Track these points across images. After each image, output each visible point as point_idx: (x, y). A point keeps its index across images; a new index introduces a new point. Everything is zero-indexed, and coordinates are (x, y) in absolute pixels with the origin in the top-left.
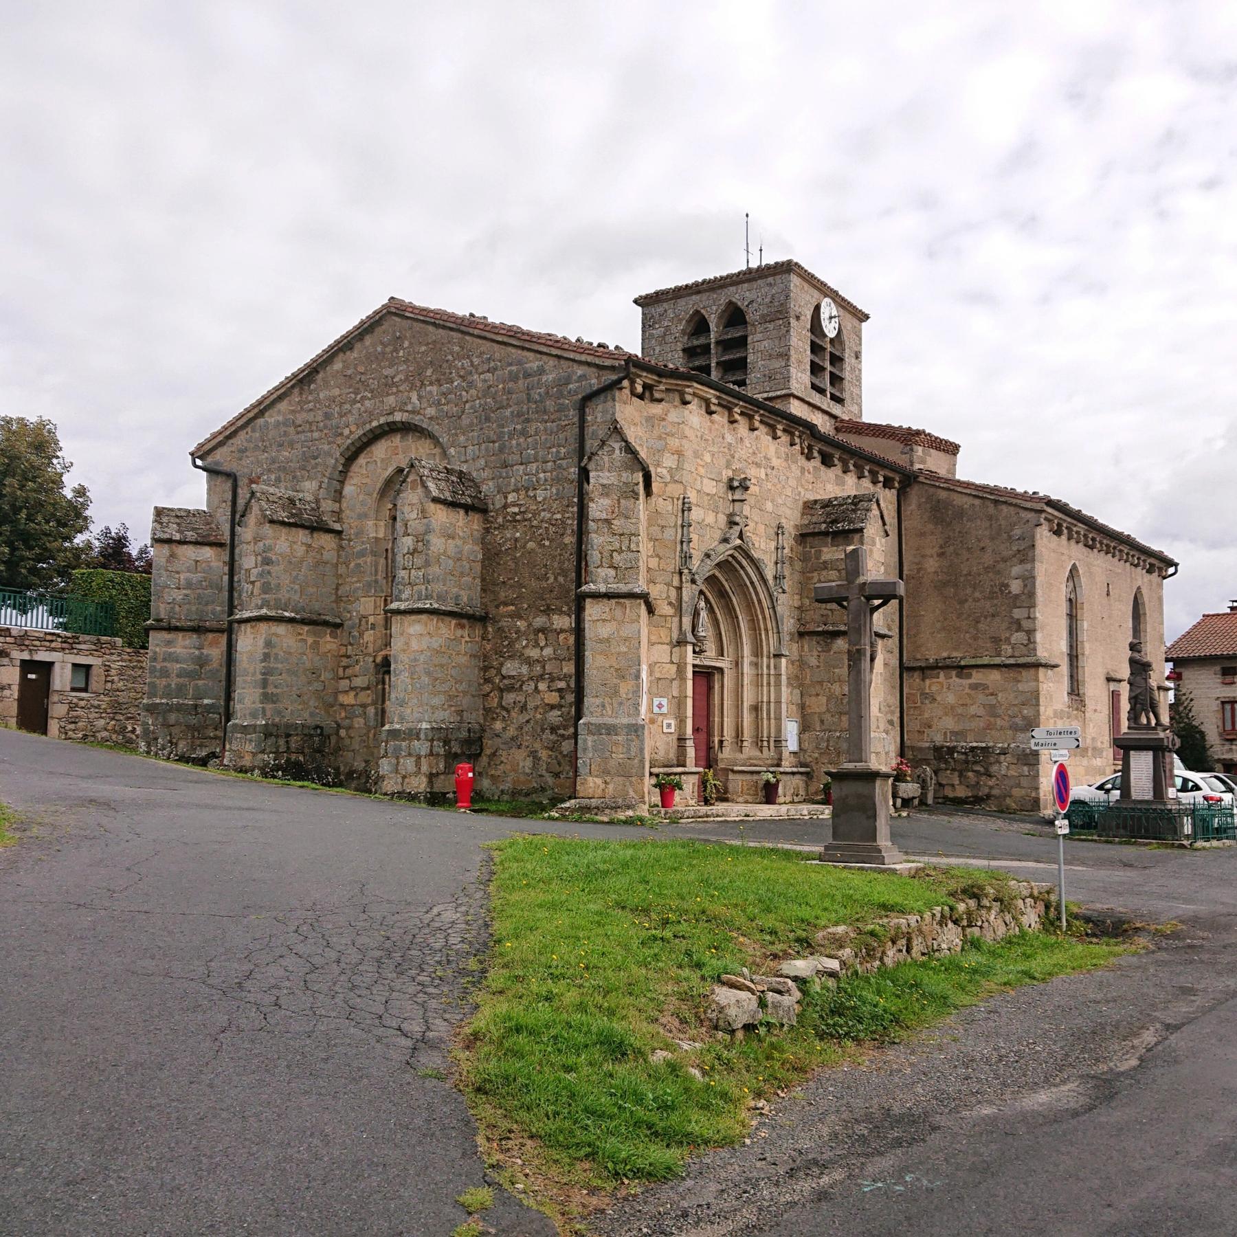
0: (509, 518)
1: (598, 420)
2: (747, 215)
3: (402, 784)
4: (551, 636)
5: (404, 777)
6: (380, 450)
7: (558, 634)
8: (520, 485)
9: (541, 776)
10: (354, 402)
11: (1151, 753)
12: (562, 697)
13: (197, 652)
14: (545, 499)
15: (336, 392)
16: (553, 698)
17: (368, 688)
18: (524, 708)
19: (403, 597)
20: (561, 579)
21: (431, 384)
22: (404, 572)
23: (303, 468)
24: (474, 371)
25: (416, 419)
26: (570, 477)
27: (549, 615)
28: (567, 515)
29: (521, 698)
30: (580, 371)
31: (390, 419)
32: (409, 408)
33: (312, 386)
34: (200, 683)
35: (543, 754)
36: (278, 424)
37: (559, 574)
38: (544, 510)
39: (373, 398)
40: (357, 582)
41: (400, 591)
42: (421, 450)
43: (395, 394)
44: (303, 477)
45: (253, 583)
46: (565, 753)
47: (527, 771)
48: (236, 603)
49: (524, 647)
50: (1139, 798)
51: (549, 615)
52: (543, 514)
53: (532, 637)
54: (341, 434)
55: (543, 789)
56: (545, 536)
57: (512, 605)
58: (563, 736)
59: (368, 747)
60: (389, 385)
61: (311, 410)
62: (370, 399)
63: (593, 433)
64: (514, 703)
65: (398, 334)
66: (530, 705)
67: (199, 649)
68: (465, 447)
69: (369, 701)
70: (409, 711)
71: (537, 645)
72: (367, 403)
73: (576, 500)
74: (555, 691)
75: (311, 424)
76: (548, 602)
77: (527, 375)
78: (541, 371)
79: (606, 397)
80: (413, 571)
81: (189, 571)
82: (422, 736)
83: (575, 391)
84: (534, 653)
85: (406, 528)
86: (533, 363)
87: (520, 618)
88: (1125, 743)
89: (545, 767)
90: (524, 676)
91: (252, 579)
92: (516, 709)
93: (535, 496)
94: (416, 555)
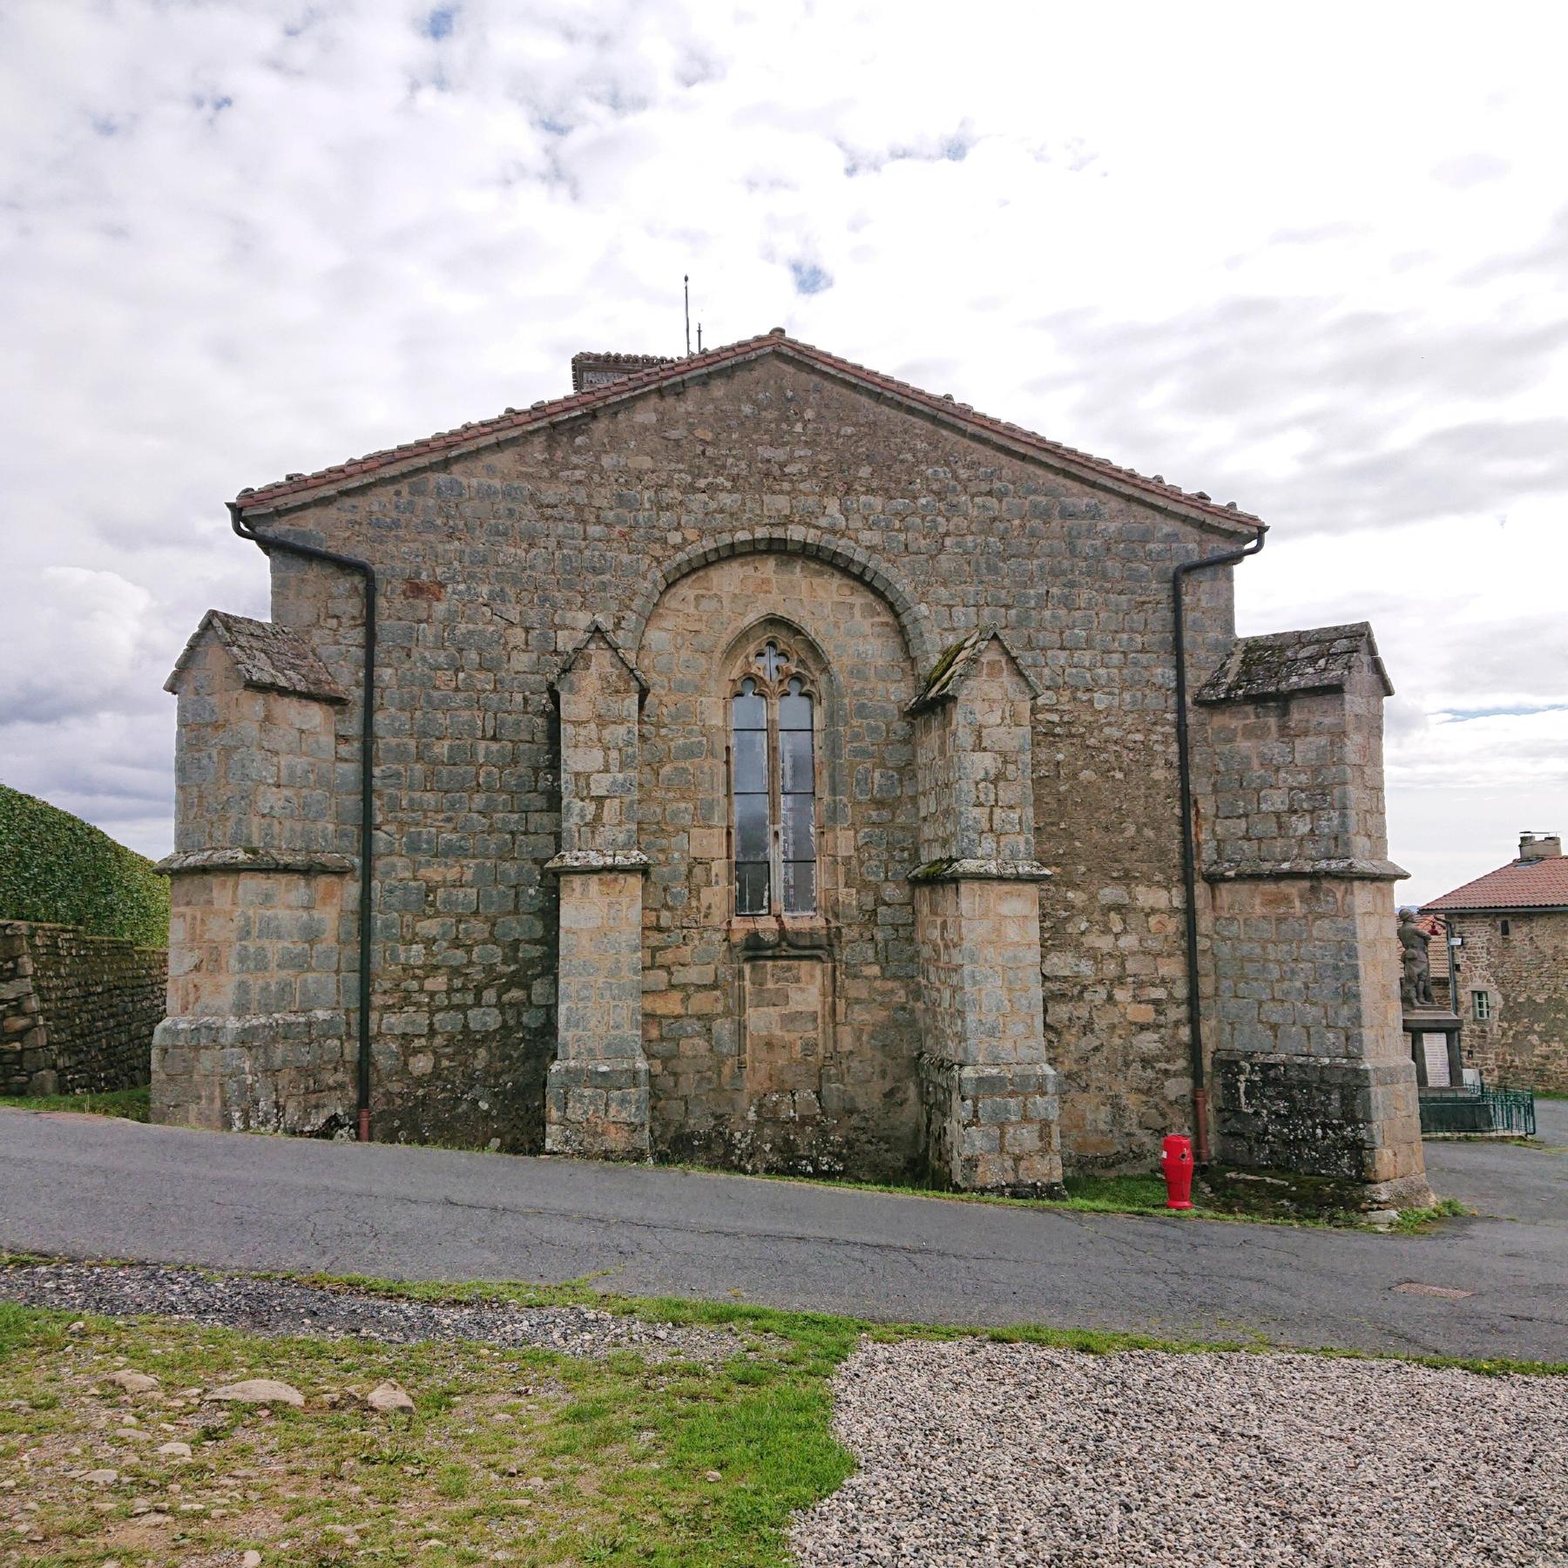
0: (1041, 729)
1: (1203, 604)
2: (686, 279)
3: (1016, 1170)
4: (1134, 921)
5: (1017, 1159)
6: (729, 579)
7: (1147, 915)
8: (1060, 681)
9: (1129, 1135)
10: (692, 489)
11: (1444, 1035)
12: (1159, 1012)
13: (305, 916)
14: (1109, 709)
16: (1146, 1014)
17: (714, 986)
18: (1088, 1028)
19: (980, 852)
20: (1149, 833)
21: (870, 491)
22: (979, 810)
24: (959, 488)
25: (841, 545)
26: (1154, 680)
27: (1128, 885)
28: (1154, 737)
29: (1083, 1012)
30: (1168, 527)
31: (778, 533)
32: (823, 522)
33: (579, 440)
34: (310, 976)
35: (1131, 1101)
37: (1145, 825)
38: (1110, 724)
40: (677, 800)
41: (971, 841)
42: (821, 593)
43: (789, 493)
44: (568, 602)
46: (1172, 1098)
47: (1102, 1126)
48: (379, 819)
49: (1083, 933)
50: (1436, 1085)
51: (1128, 885)
52: (1107, 730)
53: (1097, 916)
55: (1139, 1157)
56: (1115, 764)
57: (1057, 865)
58: (1166, 1072)
59: (719, 1089)
60: (771, 477)
61: (579, 482)
62: (729, 492)
63: (1194, 622)
64: (1070, 1019)
65: (790, 394)
66: (1101, 1023)
67: (307, 908)
68: (950, 607)
69: (720, 1008)
70: (1009, 1045)
71: (1106, 930)
72: (726, 499)
73: (1170, 717)
74: (1148, 1002)
75: (580, 509)
76: (1127, 865)
77: (1066, 514)
78: (1094, 514)
79: (1216, 574)
80: (997, 811)
81: (291, 752)
82: (1050, 1088)
83: (1159, 554)
84: (1104, 943)
85: (979, 737)
86: (1080, 498)
87: (1075, 886)
88: (1448, 1026)
89: (1135, 1121)
90: (1087, 977)
92: (1074, 1031)
93: (1091, 701)
94: (1001, 784)
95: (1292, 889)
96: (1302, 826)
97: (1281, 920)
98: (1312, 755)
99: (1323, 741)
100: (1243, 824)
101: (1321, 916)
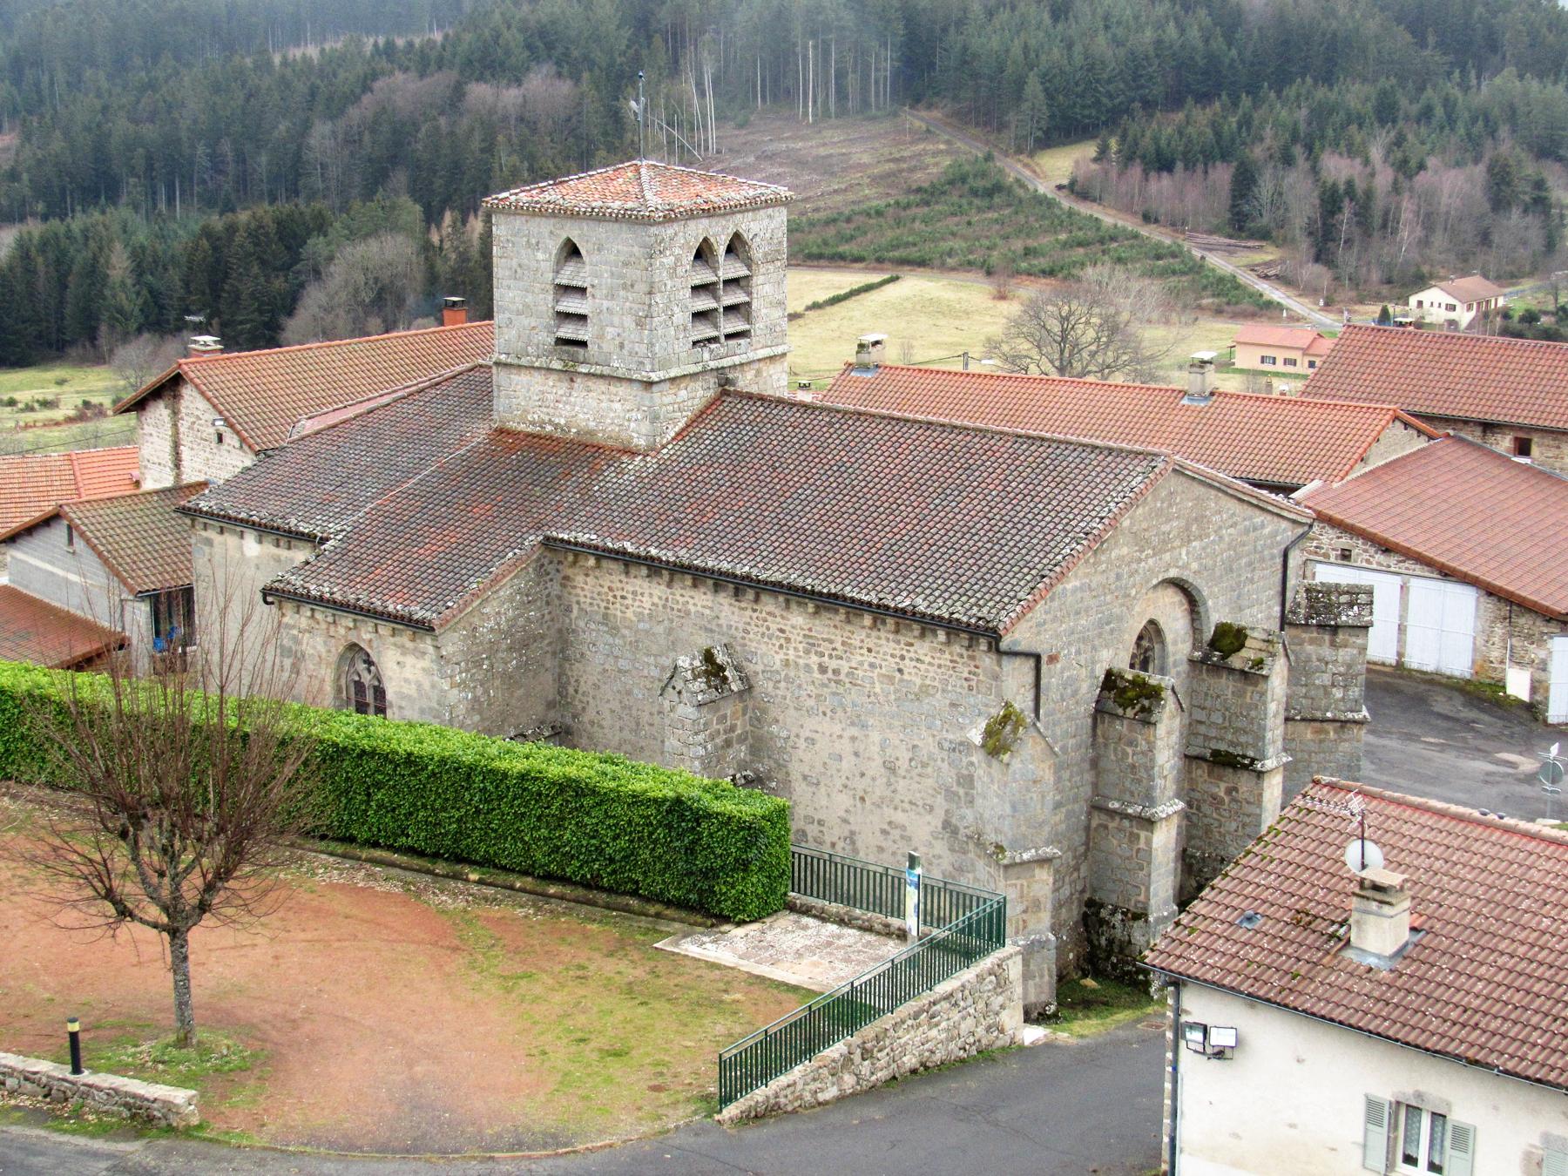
10: (1140, 560)
15: (1125, 550)
23: (1100, 635)
36: (1075, 590)
39: (1154, 555)
45: (1165, 777)
54: (1129, 595)
64: (881, 18)
72: (1151, 561)
91: (1165, 773)
95: (1330, 727)
96: (1338, 693)
97: (1321, 741)
98: (1348, 658)
99: (1355, 652)
100: (1304, 690)
101: (1345, 740)
